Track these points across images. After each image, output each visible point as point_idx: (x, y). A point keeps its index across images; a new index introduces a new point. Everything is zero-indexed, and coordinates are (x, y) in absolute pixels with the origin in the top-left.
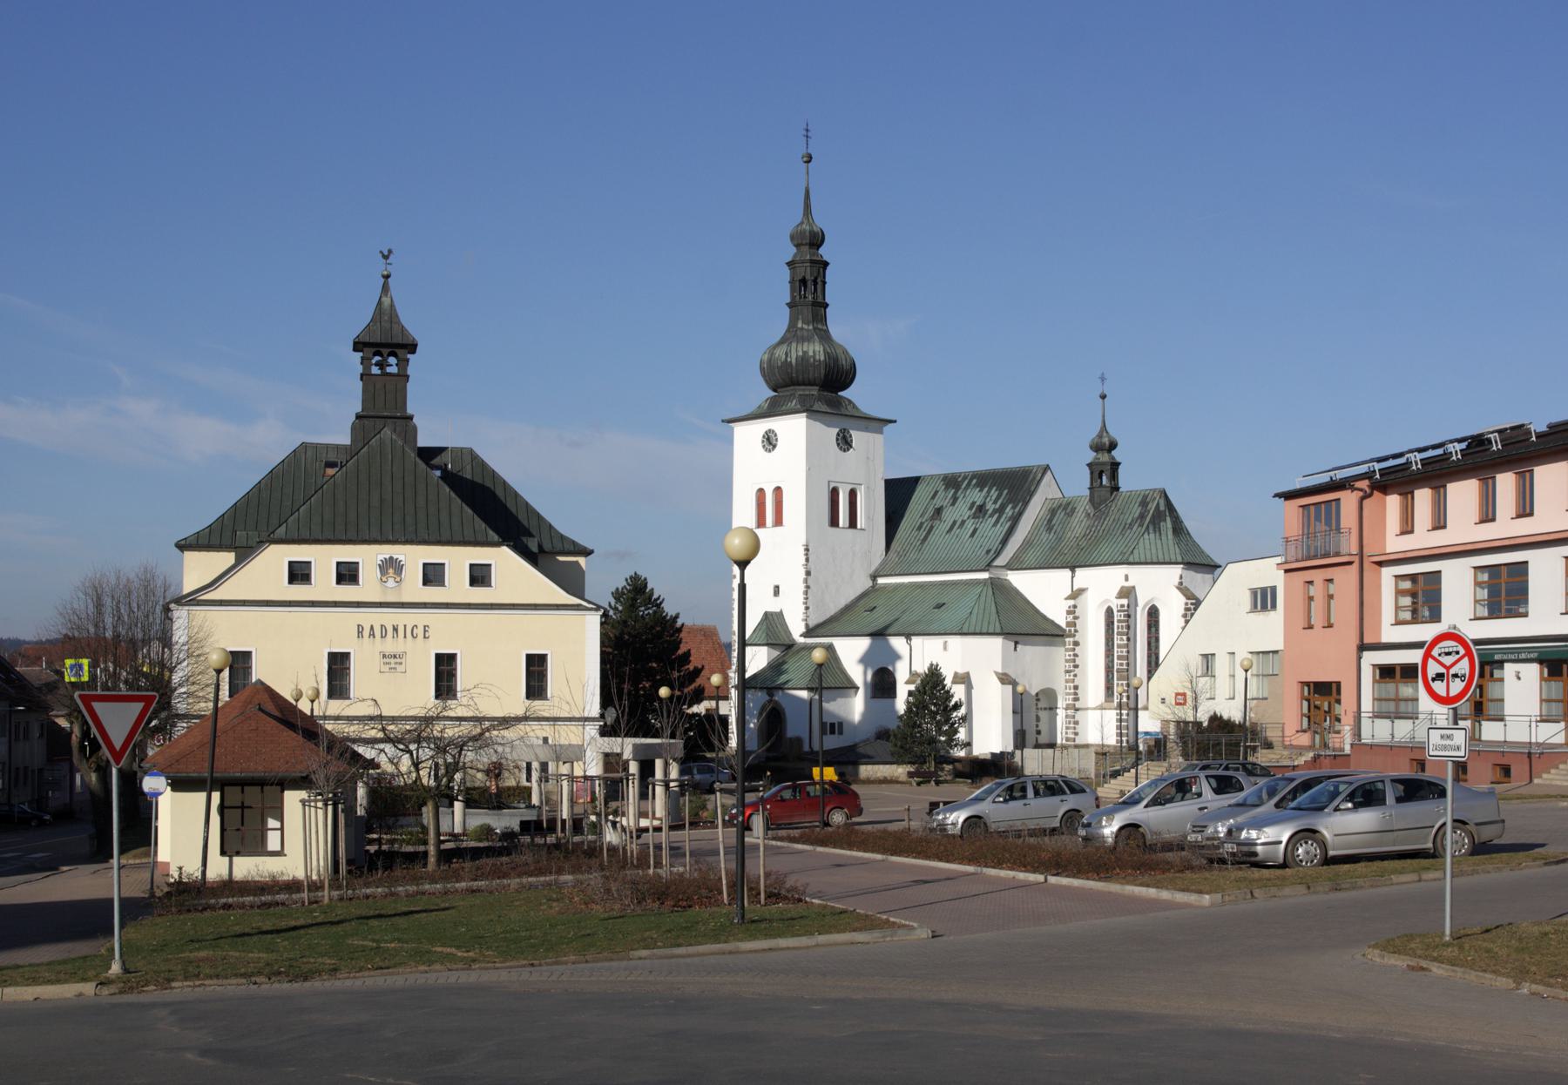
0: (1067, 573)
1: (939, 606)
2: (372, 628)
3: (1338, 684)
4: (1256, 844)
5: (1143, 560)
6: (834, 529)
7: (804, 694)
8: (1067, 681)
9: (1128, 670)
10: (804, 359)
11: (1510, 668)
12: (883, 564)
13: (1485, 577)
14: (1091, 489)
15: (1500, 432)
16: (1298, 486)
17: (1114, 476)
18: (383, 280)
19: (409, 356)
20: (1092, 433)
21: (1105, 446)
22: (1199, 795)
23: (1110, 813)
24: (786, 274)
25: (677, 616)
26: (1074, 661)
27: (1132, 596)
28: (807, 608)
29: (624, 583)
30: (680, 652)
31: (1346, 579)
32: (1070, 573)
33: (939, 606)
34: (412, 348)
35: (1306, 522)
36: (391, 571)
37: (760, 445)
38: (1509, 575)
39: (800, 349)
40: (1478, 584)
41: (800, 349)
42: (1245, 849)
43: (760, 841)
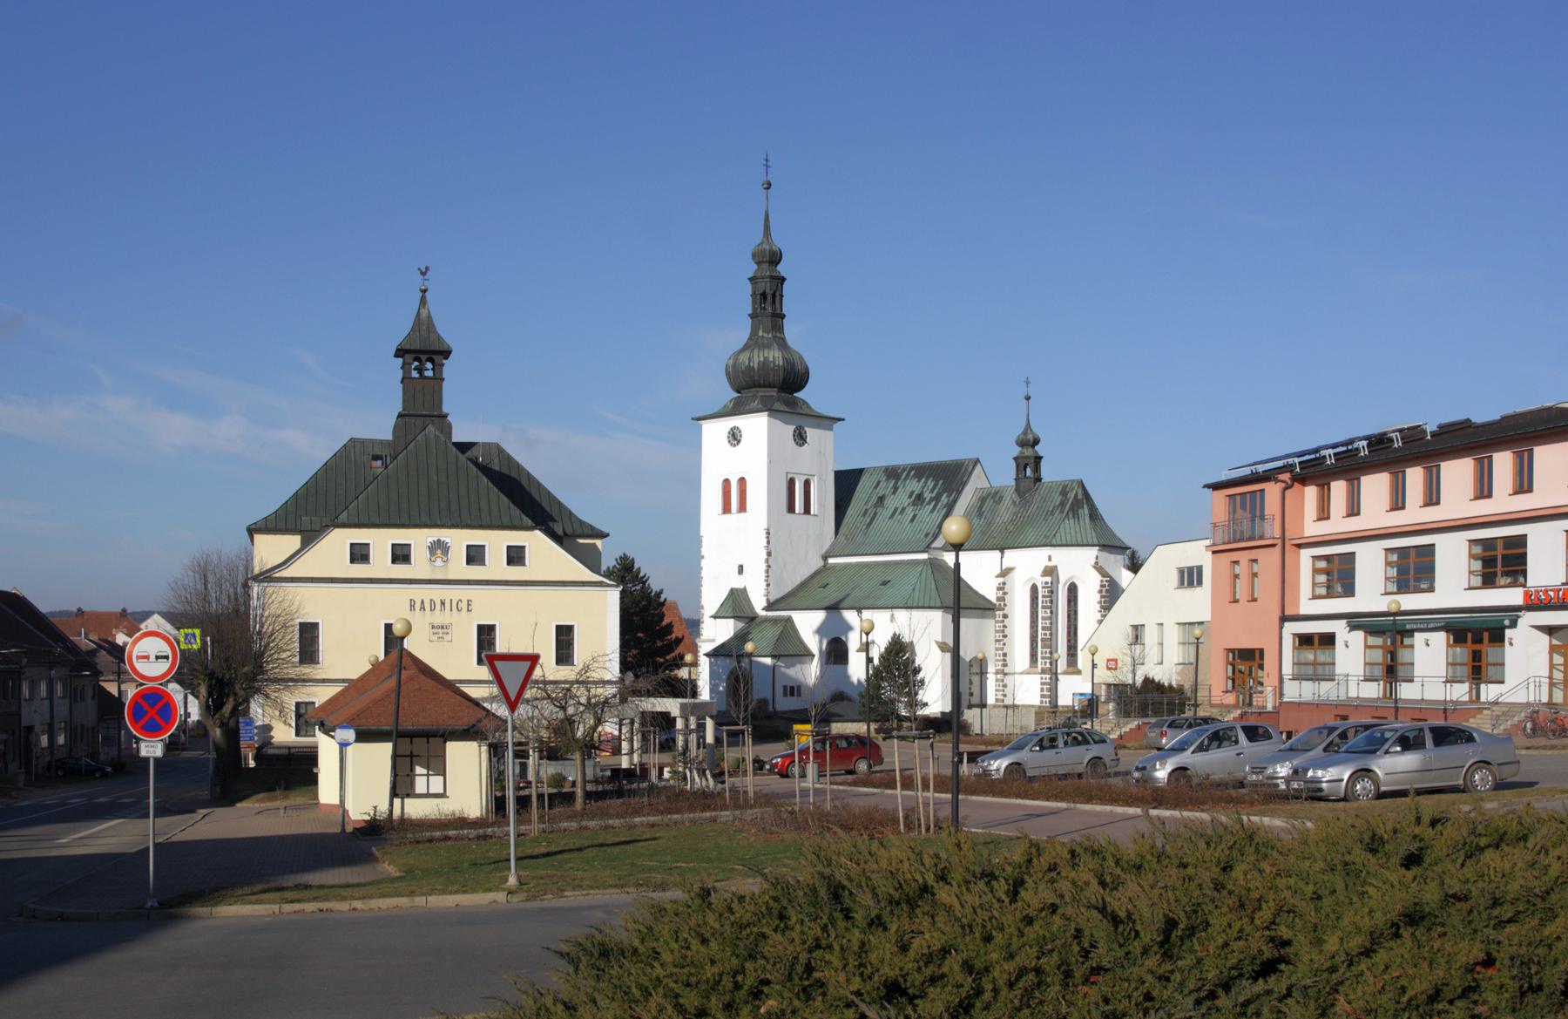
0: (997, 554)
1: (885, 583)
2: (422, 602)
3: (1261, 651)
4: (1322, 782)
5: (1064, 543)
6: (791, 515)
7: (768, 661)
8: (997, 649)
9: (1051, 640)
10: (765, 364)
11: (1419, 638)
12: (833, 546)
13: (1394, 558)
14: (1017, 479)
15: (1400, 431)
16: (1224, 478)
17: (1037, 468)
18: (421, 294)
19: (444, 361)
20: (1018, 431)
21: (1029, 441)
22: (1237, 742)
23: (1163, 759)
24: (748, 287)
25: (661, 592)
26: (1003, 631)
27: (1055, 574)
28: (768, 585)
29: (615, 563)
30: (664, 623)
31: (1269, 559)
32: (1000, 554)
33: (885, 583)
34: (446, 354)
35: (1233, 510)
36: (439, 552)
37: (726, 440)
38: (1417, 556)
39: (761, 355)
40: (1388, 564)
41: (761, 355)
42: (1314, 785)
43: (811, 785)
